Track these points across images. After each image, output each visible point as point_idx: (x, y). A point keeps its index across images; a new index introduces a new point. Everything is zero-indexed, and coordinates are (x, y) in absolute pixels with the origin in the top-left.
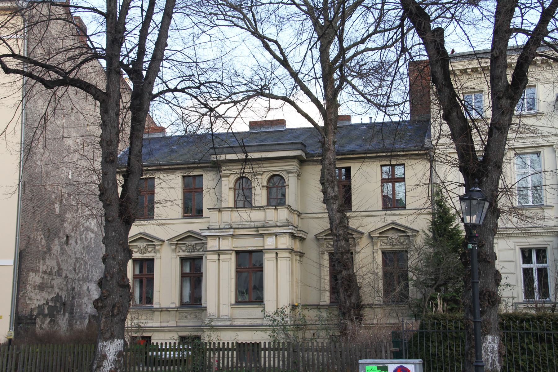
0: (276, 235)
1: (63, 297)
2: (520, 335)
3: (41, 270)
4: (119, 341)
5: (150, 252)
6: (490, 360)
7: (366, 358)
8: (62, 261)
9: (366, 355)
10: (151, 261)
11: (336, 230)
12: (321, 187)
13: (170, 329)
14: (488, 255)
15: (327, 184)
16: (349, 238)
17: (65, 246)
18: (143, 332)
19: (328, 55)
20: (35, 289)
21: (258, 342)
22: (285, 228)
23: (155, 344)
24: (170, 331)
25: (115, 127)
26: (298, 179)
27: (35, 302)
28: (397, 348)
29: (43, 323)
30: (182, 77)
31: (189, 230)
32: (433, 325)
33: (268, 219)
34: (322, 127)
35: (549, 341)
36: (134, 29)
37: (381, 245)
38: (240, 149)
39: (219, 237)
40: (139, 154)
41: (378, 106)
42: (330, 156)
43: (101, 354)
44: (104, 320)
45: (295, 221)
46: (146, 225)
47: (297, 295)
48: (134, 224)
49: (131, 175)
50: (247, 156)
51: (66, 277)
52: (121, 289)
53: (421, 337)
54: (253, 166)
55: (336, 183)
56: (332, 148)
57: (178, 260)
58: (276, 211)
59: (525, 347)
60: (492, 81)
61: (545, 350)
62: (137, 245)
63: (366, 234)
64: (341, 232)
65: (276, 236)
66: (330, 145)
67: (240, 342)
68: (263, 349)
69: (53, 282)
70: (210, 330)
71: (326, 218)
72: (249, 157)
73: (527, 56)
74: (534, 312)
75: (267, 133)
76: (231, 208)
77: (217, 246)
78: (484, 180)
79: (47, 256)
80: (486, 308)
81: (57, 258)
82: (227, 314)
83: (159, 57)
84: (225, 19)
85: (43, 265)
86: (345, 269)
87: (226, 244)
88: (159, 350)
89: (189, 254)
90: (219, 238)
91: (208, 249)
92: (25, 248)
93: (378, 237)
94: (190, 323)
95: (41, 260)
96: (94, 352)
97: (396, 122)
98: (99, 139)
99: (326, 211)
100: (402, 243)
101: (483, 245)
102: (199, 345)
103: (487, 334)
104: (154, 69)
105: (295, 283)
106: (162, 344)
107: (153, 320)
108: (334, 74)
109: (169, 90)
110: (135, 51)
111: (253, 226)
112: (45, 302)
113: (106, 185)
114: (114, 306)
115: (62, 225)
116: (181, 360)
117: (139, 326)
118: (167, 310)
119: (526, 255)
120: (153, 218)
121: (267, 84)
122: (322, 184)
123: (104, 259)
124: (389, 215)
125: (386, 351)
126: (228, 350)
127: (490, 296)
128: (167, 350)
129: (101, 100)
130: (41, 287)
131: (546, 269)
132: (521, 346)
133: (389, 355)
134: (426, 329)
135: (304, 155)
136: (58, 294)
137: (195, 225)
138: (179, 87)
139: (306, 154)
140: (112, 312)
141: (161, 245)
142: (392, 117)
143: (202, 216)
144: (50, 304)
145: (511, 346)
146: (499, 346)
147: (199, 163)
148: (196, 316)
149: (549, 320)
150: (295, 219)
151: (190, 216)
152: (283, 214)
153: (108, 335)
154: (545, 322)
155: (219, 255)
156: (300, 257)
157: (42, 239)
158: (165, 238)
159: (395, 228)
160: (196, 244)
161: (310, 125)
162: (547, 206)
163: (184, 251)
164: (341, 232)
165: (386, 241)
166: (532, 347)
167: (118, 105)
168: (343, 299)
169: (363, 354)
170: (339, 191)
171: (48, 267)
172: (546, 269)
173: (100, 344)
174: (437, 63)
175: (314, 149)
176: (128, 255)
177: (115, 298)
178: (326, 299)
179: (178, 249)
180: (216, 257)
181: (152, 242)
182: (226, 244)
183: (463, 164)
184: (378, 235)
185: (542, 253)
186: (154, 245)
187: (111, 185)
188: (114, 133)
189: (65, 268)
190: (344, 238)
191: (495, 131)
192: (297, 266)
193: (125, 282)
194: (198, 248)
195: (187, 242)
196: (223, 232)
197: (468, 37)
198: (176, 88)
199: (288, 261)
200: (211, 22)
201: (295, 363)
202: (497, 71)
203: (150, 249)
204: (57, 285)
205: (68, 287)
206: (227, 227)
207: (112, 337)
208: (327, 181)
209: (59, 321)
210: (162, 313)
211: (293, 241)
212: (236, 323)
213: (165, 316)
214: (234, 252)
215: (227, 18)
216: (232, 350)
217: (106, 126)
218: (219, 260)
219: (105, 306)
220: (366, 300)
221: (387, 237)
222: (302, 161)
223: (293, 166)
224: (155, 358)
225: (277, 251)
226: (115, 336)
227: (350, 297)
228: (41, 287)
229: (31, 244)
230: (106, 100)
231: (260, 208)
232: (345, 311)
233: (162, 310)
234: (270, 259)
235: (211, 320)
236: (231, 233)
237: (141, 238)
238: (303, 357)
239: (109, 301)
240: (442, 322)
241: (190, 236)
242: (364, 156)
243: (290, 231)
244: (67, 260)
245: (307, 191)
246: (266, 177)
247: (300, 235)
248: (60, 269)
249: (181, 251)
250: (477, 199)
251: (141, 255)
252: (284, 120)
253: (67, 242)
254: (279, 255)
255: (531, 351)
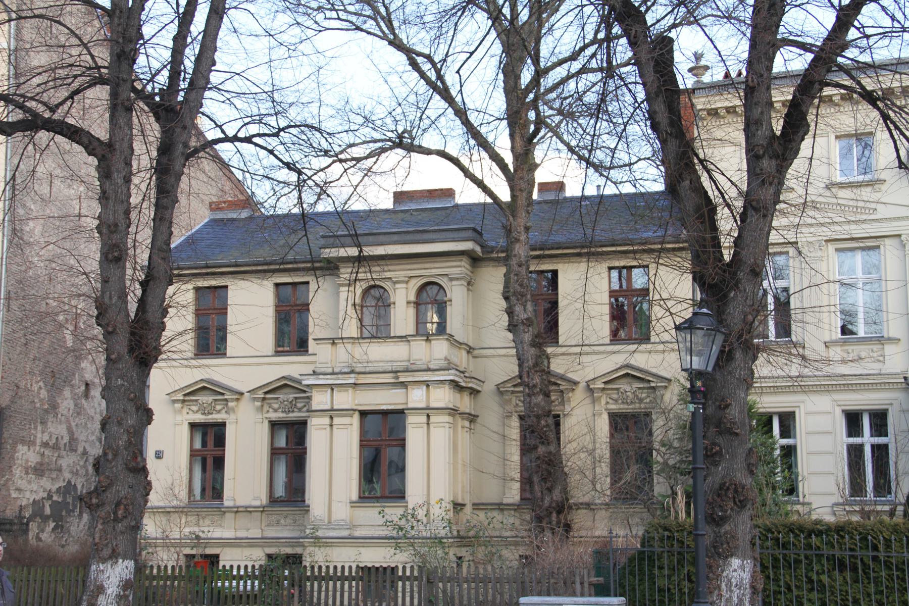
0: (427, 384)
1: (79, 487)
2: (806, 557)
3: (38, 441)
4: (126, 562)
5: (219, 412)
6: (735, 600)
7: (549, 595)
8: (77, 425)
9: (548, 590)
10: (221, 427)
11: (528, 376)
12: (504, 304)
13: (251, 543)
14: (735, 423)
15: (513, 299)
16: (550, 392)
17: (83, 401)
18: (205, 547)
19: (518, 77)
20: (27, 473)
21: (393, 565)
22: (442, 372)
23: (228, 568)
24: (251, 546)
25: (122, 202)
26: (468, 290)
27: (28, 495)
28: (601, 579)
29: (43, 531)
30: (251, 117)
31: (203, 377)
32: (662, 540)
33: (415, 357)
34: (505, 203)
35: (854, 569)
36: (153, 36)
37: (608, 403)
38: (349, 240)
39: (332, 387)
40: (164, 247)
41: (598, 168)
42: (520, 250)
43: (95, 585)
44: (100, 527)
45: (461, 362)
46: (174, 367)
47: (463, 487)
48: (155, 365)
49: (151, 283)
50: (361, 251)
51: (85, 453)
52: (131, 475)
53: (641, 559)
54: (373, 269)
55: (529, 297)
56: (523, 238)
57: (266, 425)
58: (428, 344)
59: (815, 577)
60: (747, 130)
61: (847, 583)
62: (196, 400)
63: (582, 385)
64: (537, 380)
65: (428, 386)
66: (519, 233)
67: (361, 565)
68: (400, 578)
69: (60, 462)
70: (314, 544)
71: (512, 356)
72: (365, 254)
73: (809, 85)
74: (855, 518)
75: (423, 214)
76: (352, 338)
77: (329, 403)
78: (732, 295)
79: (50, 417)
80: (729, 512)
81: (68, 421)
82: (344, 517)
83: (202, 83)
84: (339, 18)
85: (43, 432)
86: (543, 443)
87: (344, 399)
88: (234, 578)
89: (284, 415)
90: (332, 389)
91: (314, 408)
92: (9, 403)
93: (604, 389)
94: (284, 532)
95: (39, 425)
96: (84, 581)
97: (627, 195)
98: (96, 222)
99: (513, 344)
100: (641, 401)
101: (727, 406)
102: (272, 571)
103: (732, 556)
104: (194, 105)
105: (460, 466)
106: (239, 567)
107: (223, 527)
108: (524, 113)
109: (227, 139)
110: (166, 73)
111: (390, 369)
112: (45, 495)
113: (107, 300)
114: (118, 504)
115: (77, 365)
116: (241, 596)
117: (198, 537)
118: (247, 510)
119: (853, 420)
120: (224, 355)
121: (409, 129)
122: (506, 298)
123: (104, 425)
124: (588, 354)
125: (582, 583)
126: (343, 578)
127: (736, 491)
128: (241, 578)
129: (100, 156)
130: (39, 470)
131: (886, 446)
132: (806, 576)
133: (586, 589)
134: (651, 546)
135: (478, 249)
136: (69, 482)
137: (293, 367)
138: (241, 135)
139: (482, 246)
140: (115, 513)
141: (238, 400)
142: (620, 187)
143: (307, 351)
144: (55, 498)
145: (791, 576)
146: (752, 577)
147: (281, 264)
148: (295, 521)
149: (855, 533)
150: (461, 358)
151: (287, 351)
152: (440, 349)
153: (106, 552)
154: (847, 536)
155: (331, 418)
156: (471, 422)
157: (40, 388)
158: (243, 389)
159: (631, 375)
160: (296, 398)
161: (489, 200)
162: (889, 339)
163: (276, 411)
164: (537, 380)
165: (615, 396)
166: (825, 578)
167: (129, 164)
168: (539, 494)
169: (545, 588)
170: (535, 311)
171: (51, 436)
172: (886, 446)
173: (94, 567)
174: (657, 96)
175: (496, 239)
176: (144, 418)
177: (121, 490)
178: (513, 494)
179: (266, 408)
180: (327, 421)
181: (223, 394)
182: (344, 399)
183: (698, 269)
184: (602, 386)
185: (880, 420)
186: (226, 400)
187: (114, 300)
188: (121, 212)
189: (82, 437)
190: (541, 390)
191: (751, 212)
192: (464, 437)
193: (138, 463)
194: (299, 405)
195: (281, 396)
196: (339, 379)
197: (719, 52)
198: (235, 136)
199: (447, 429)
200: (316, 22)
201: (430, 601)
202: (754, 111)
203: (218, 407)
204: (68, 466)
205: (87, 471)
206: (346, 370)
207: (114, 556)
208: (515, 294)
209: (72, 528)
210: (238, 514)
211: (458, 395)
212: (358, 533)
213: (243, 520)
214: (357, 414)
215: (343, 15)
216: (350, 578)
217: (107, 199)
218: (331, 425)
219: (103, 504)
220: (580, 493)
221: (617, 389)
222: (475, 260)
223: (460, 267)
224: (219, 592)
225: (428, 411)
226: (119, 554)
227: (550, 490)
228: (39, 470)
229: (21, 397)
230: (110, 157)
231: (404, 338)
232: (542, 514)
233: (237, 510)
234: (417, 425)
235: (315, 529)
236: (352, 381)
237: (204, 388)
238: (444, 591)
239: (110, 496)
240: (676, 534)
241: (285, 385)
242: (587, 250)
243: (452, 378)
244: (86, 424)
245: (481, 310)
246: (415, 284)
247: (470, 385)
248: (73, 440)
249: (271, 410)
250: (703, 329)
251: (204, 417)
252: (451, 189)
253: (86, 395)
254: (432, 419)
255: (824, 586)
